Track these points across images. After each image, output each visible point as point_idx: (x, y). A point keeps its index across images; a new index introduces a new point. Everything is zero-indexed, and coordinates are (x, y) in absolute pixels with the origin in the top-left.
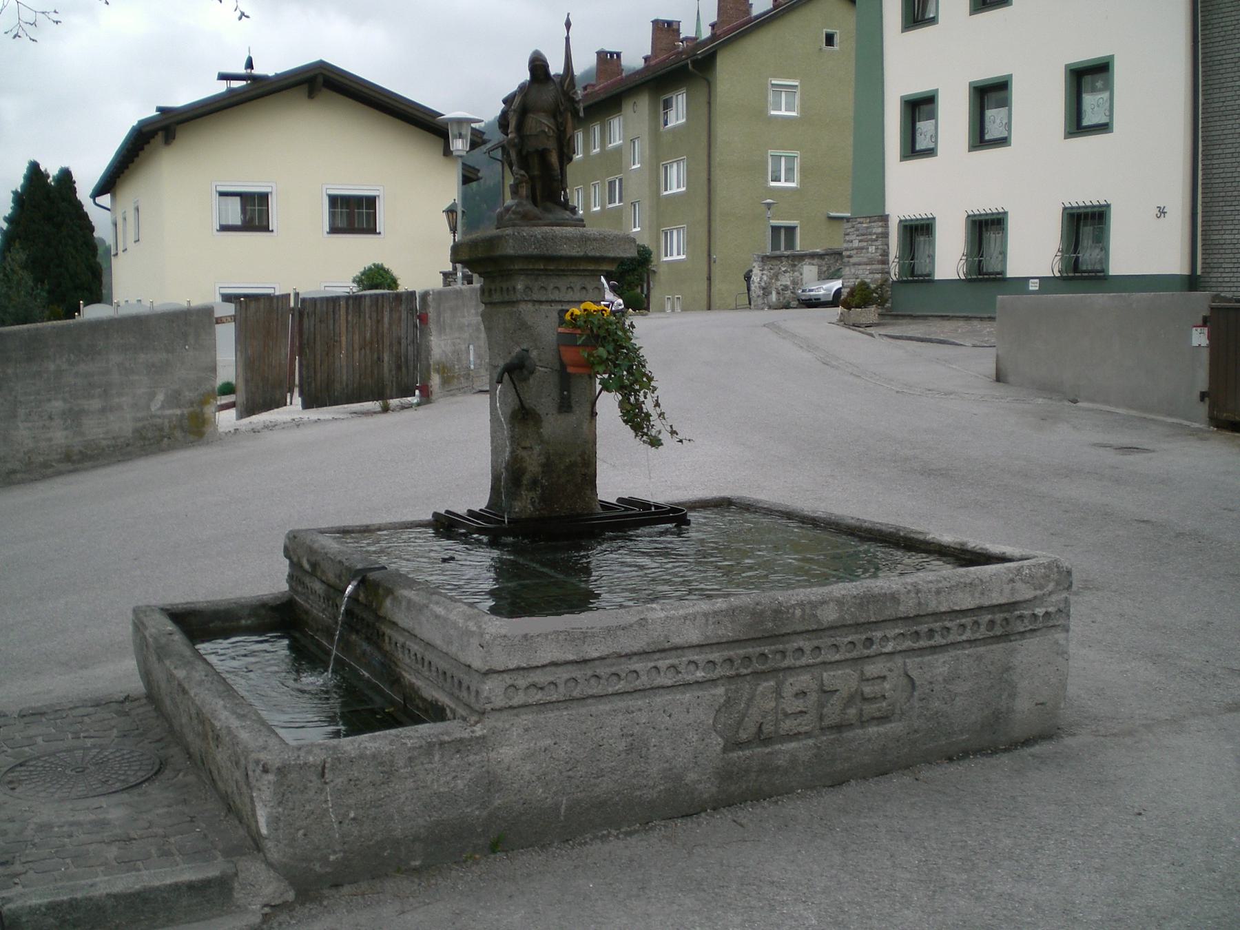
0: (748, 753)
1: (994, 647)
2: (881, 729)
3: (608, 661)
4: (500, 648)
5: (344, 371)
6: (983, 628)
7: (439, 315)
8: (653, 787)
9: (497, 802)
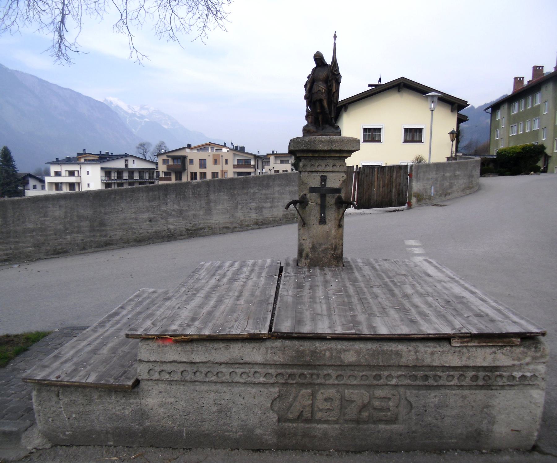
0: (295, 425)
1: (477, 392)
2: (388, 427)
3: (208, 365)
4: (145, 350)
5: (375, 195)
6: (468, 380)
7: (417, 174)
8: (236, 432)
9: (147, 424)
